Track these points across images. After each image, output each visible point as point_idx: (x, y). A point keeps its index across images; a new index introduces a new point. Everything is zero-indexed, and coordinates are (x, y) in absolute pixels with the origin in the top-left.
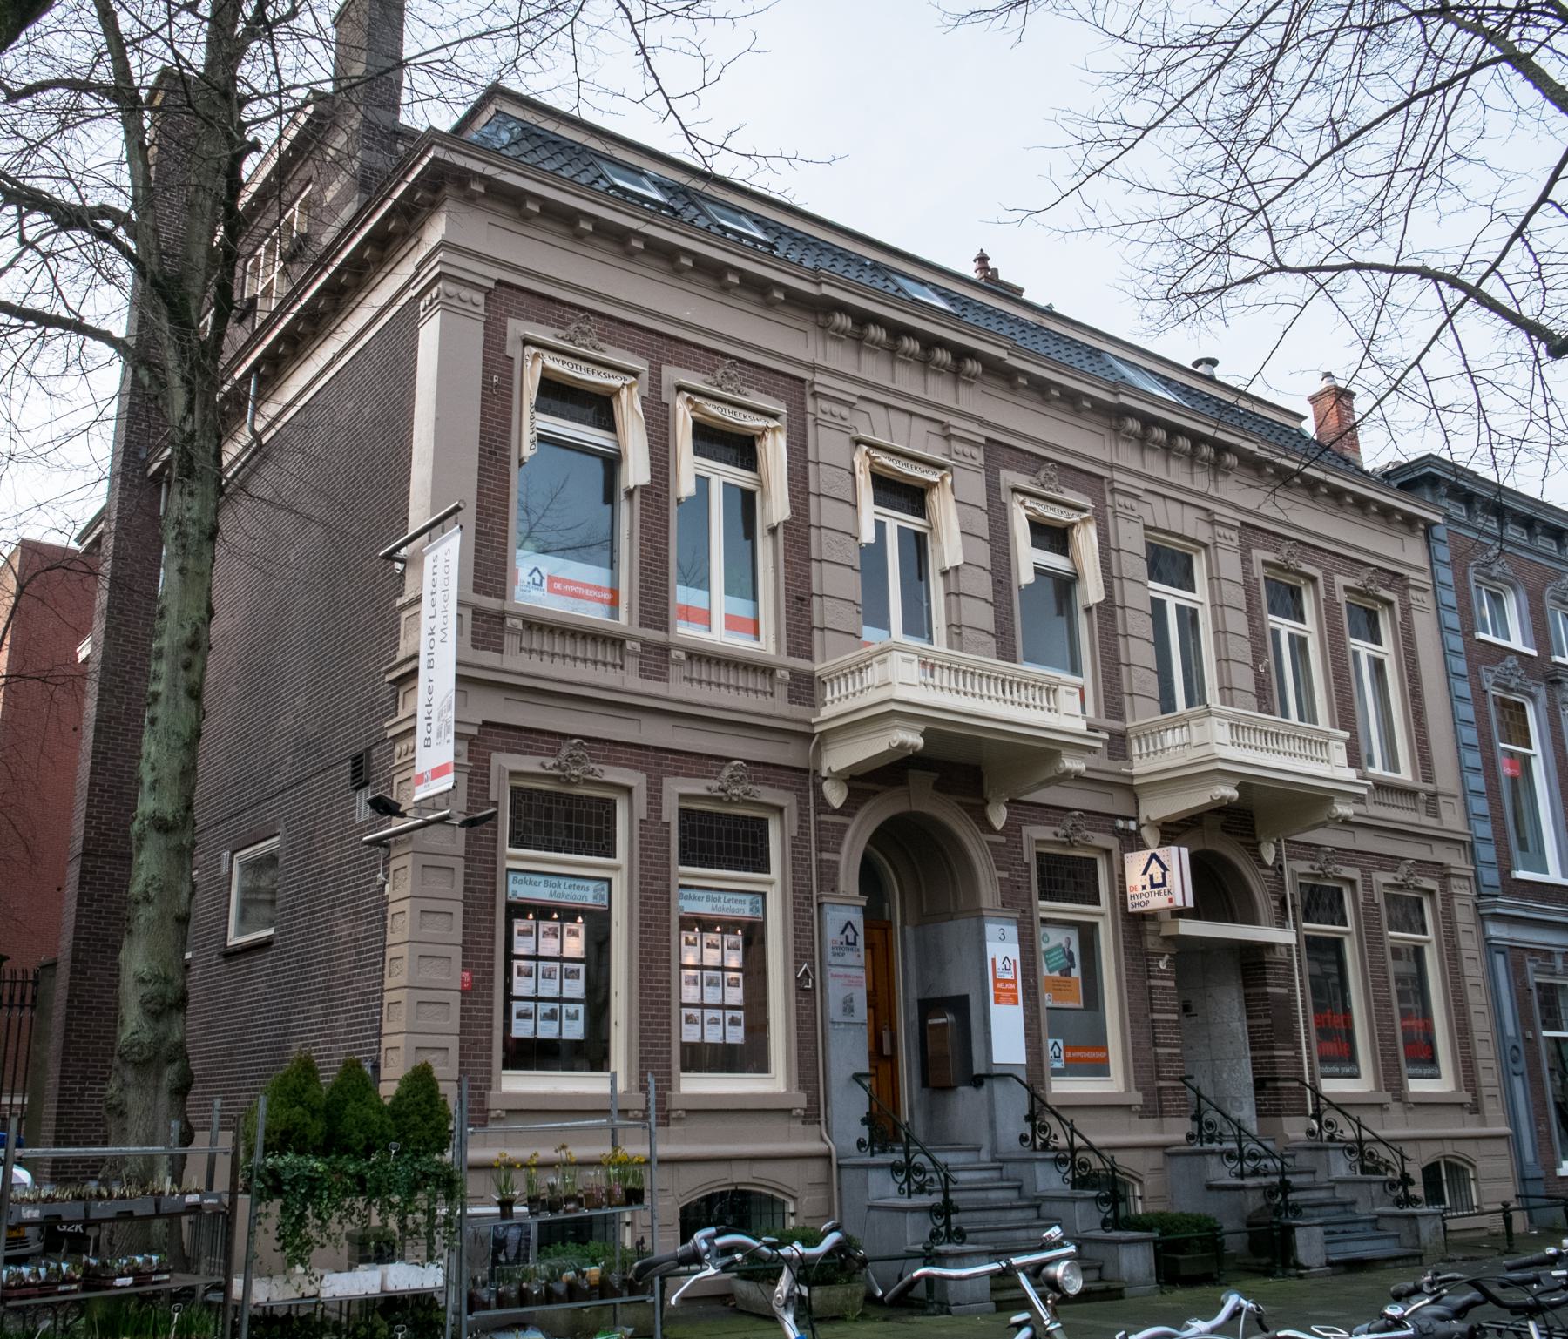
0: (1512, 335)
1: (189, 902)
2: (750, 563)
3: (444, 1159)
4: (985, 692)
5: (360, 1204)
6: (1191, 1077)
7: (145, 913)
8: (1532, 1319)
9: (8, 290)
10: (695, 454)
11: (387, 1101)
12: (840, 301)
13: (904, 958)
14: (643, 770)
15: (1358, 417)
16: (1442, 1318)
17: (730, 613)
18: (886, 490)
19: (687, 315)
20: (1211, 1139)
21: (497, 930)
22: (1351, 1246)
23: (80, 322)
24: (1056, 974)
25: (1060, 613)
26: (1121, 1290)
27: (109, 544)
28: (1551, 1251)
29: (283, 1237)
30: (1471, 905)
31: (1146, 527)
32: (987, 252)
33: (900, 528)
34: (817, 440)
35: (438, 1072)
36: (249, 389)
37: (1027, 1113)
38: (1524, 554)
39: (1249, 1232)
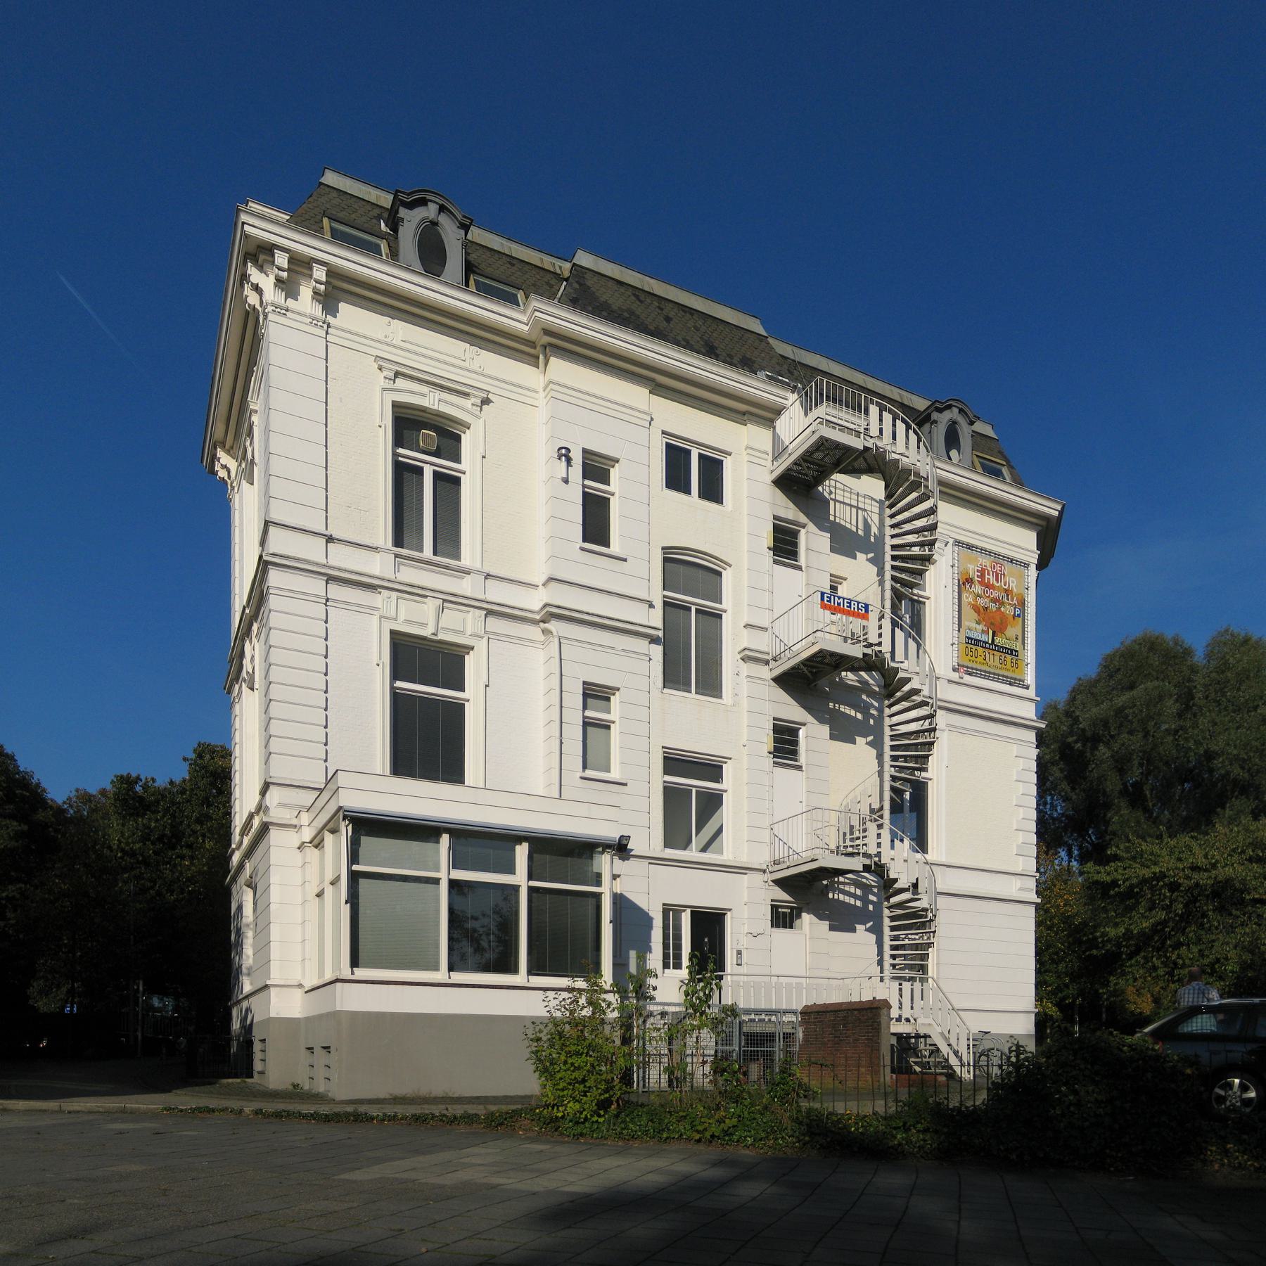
0: (658, 664)
1: (233, 444)
2: (504, 584)
3: (902, 1134)
4: (484, 256)
5: (1119, 1017)
6: (925, 863)
7: (811, 1104)
8: (37, 791)
9: (312, 853)
10: (585, 539)
11: (1101, 744)
12: (681, 927)
13: (596, 462)
14: (628, 952)
15: (798, 400)
16: (601, 1094)
17: (607, 703)
18: (1057, 520)
19: (606, 878)
20: (744, 1059)
21: (404, 870)
22: (899, 505)
23: (13, 757)
24: (884, 1127)
25: (853, 826)
26: (892, 538)
27: (836, 471)
28: (864, 1063)
29: (539, 1040)
30: (659, 604)
31: (831, 575)
32: (533, 1072)
33: (607, 545)
34: (593, 615)
35: (782, 514)
36: (138, 987)
37: (333, 536)
38: (933, 607)
39: (771, 905)
